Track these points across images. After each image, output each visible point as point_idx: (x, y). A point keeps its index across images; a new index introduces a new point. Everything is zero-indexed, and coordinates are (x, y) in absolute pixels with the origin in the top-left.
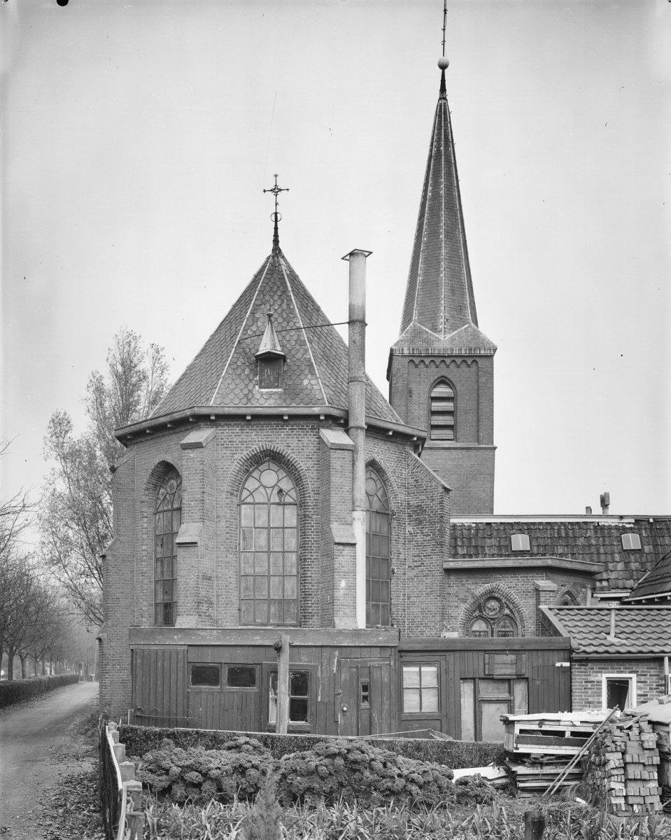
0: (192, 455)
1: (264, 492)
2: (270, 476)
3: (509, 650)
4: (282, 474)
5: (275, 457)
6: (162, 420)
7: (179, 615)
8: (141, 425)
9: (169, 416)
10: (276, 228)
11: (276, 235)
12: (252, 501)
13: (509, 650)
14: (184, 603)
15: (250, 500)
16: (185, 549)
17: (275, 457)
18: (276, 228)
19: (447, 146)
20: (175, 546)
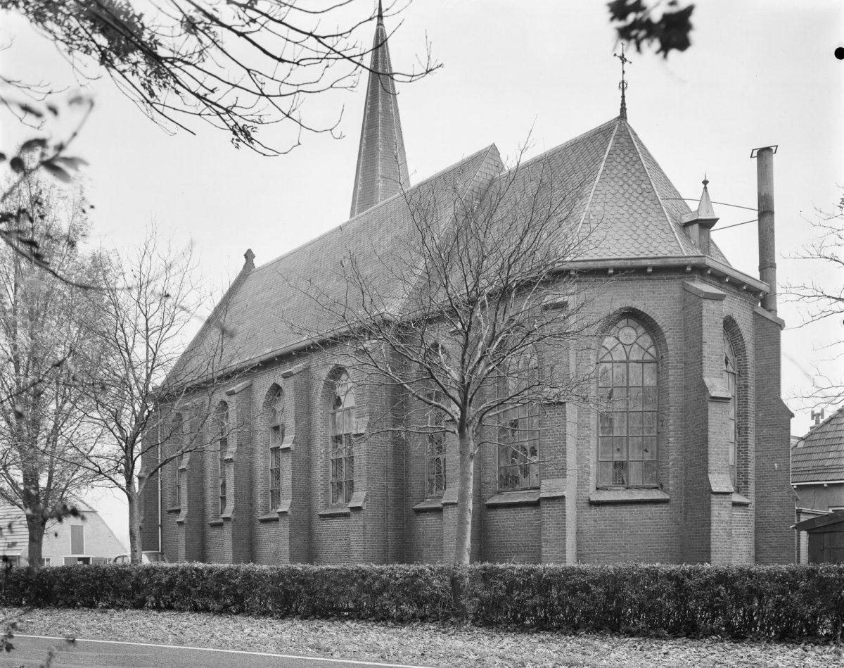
0: (712, 306)
1: (622, 349)
2: (628, 333)
3: (627, 393)
4: (641, 330)
5: (633, 315)
6: (644, 262)
7: (711, 473)
8: (640, 261)
9: (660, 260)
10: (623, 97)
11: (623, 104)
12: (611, 359)
13: (627, 393)
14: (715, 460)
15: (608, 358)
16: (717, 404)
17: (633, 315)
18: (623, 97)
19: (386, 103)
20: (316, 520)
